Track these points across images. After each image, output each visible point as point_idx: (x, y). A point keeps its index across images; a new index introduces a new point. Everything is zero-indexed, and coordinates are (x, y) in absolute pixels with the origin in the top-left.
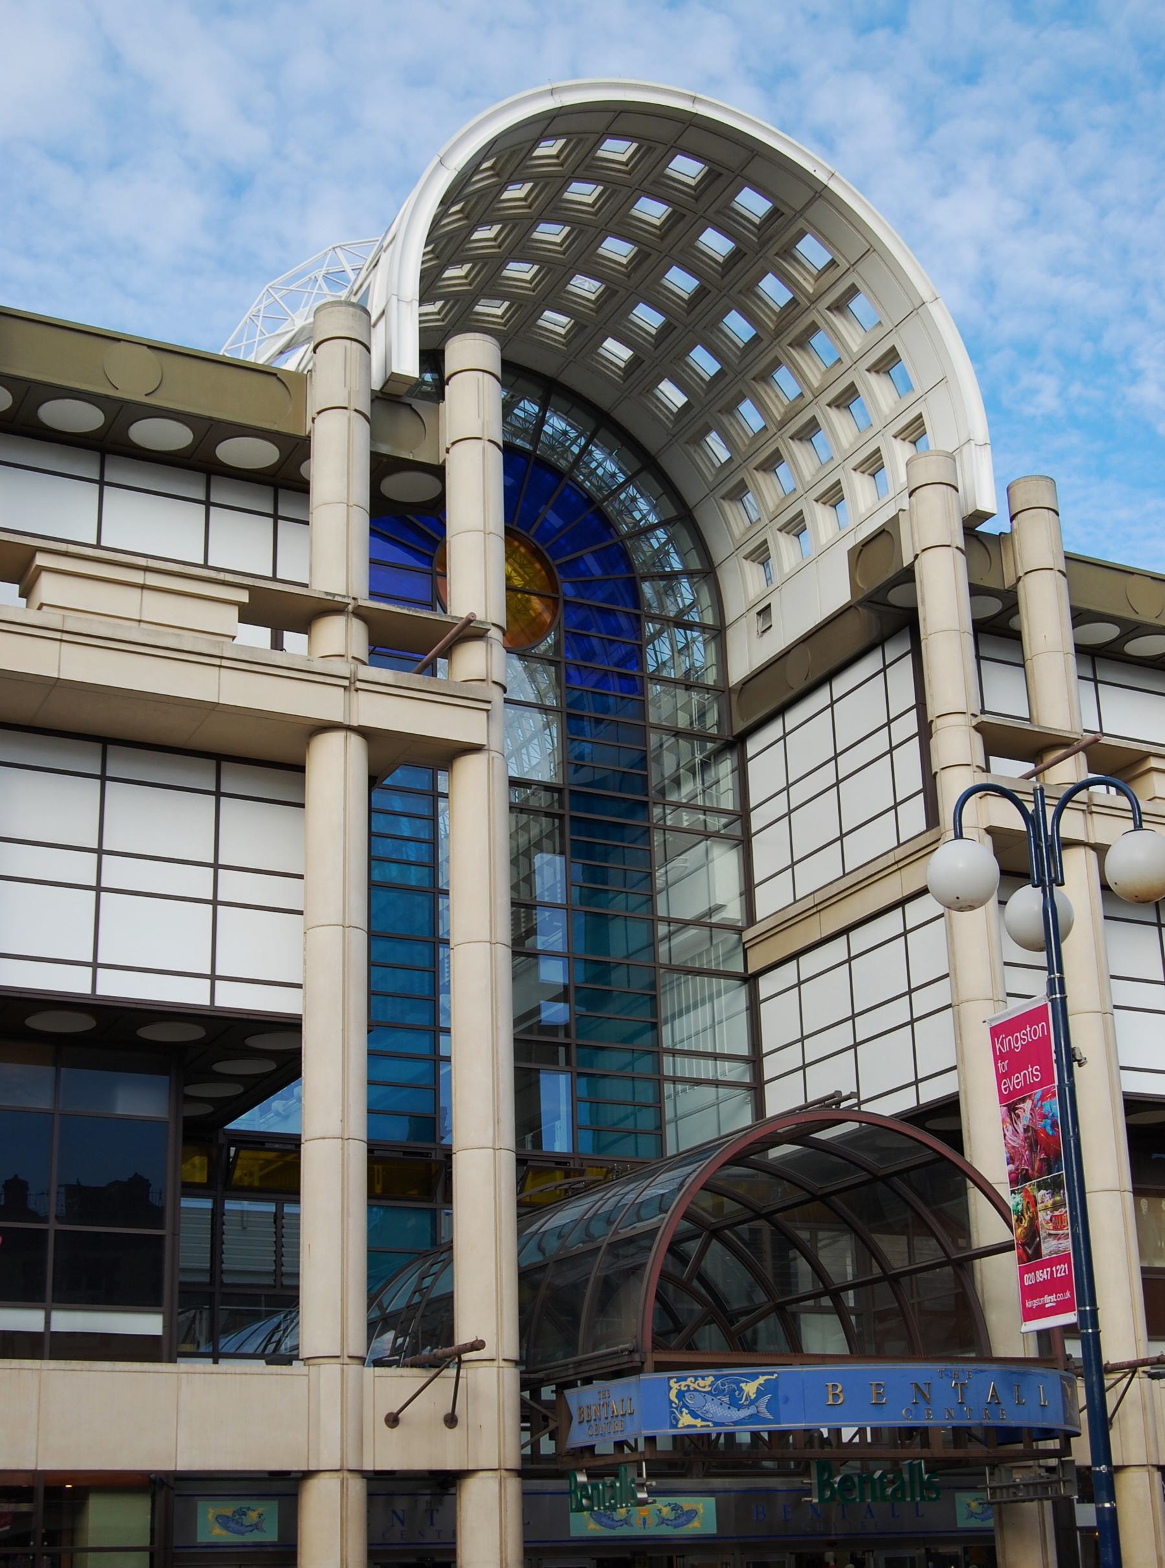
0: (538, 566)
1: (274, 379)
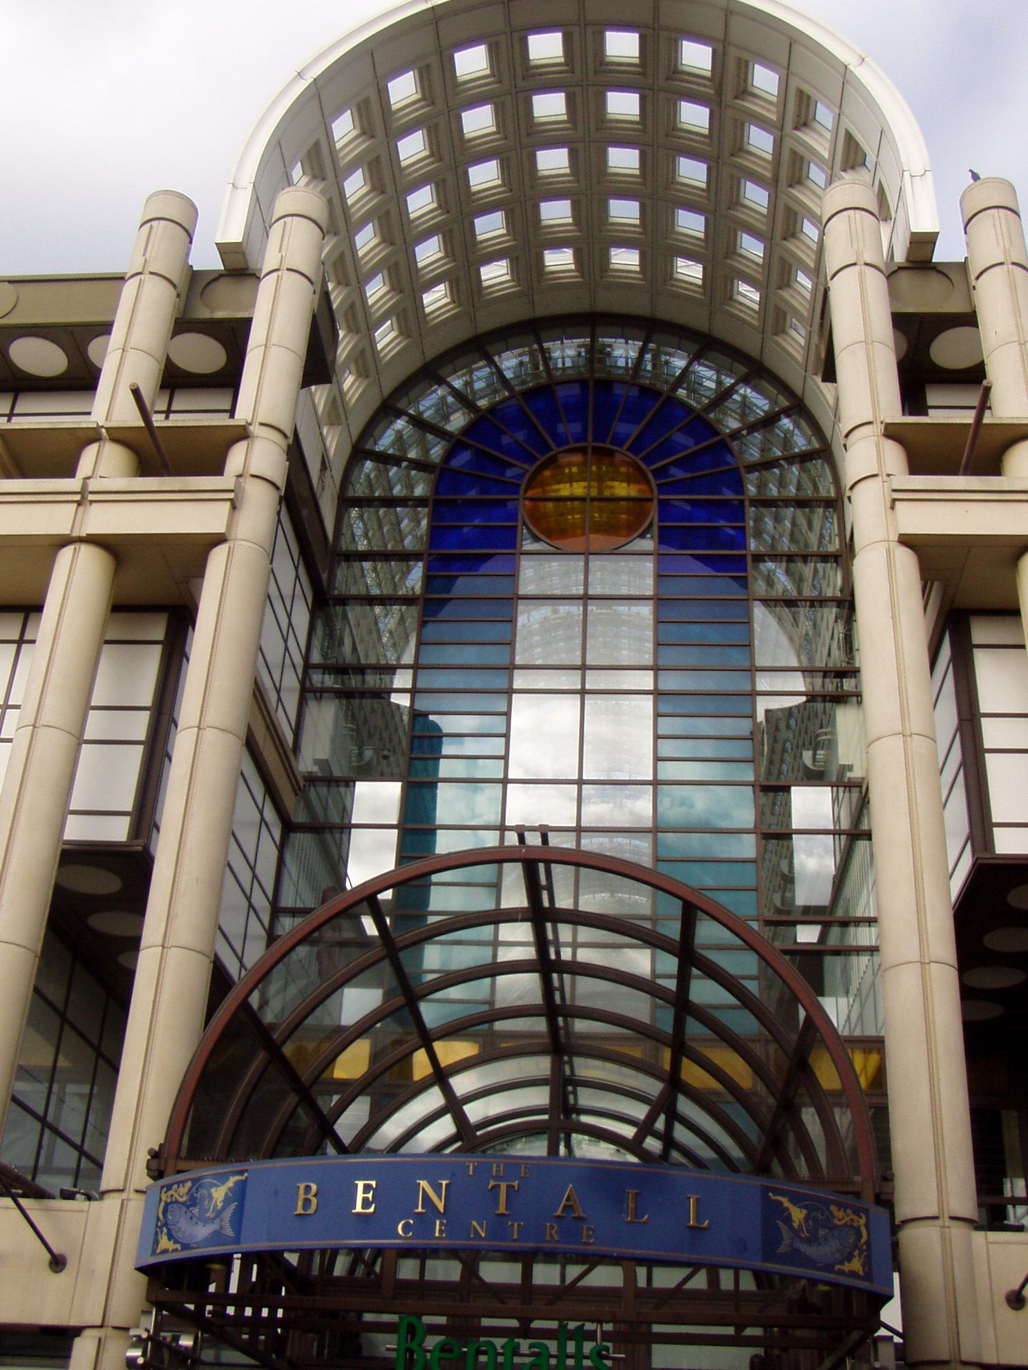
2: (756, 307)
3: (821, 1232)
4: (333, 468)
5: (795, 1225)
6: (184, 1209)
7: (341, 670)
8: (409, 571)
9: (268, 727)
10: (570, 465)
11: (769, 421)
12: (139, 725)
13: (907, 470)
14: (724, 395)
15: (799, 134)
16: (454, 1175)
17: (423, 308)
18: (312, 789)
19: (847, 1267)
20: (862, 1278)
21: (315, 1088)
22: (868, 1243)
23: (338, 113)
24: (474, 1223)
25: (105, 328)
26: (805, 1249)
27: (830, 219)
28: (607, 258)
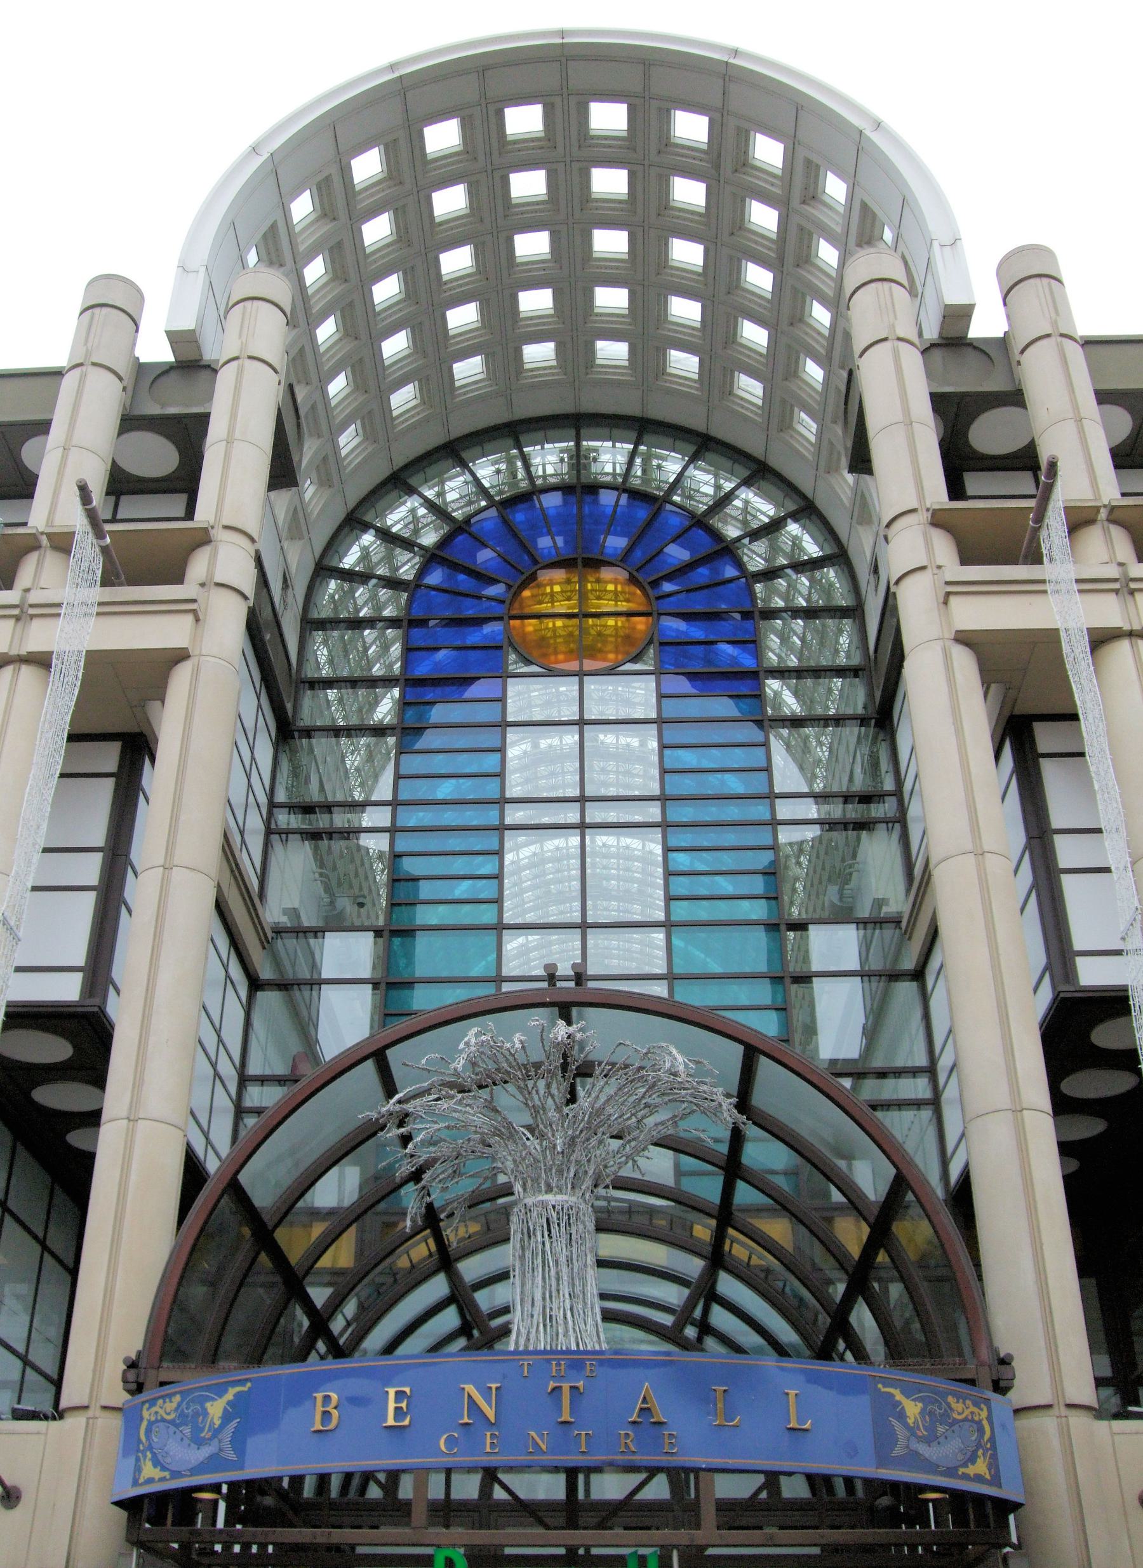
2: (760, 403)
3: (941, 1429)
4: (296, 588)
5: (911, 1421)
6: (172, 1429)
7: (308, 809)
8: (377, 702)
9: (232, 871)
10: (551, 583)
11: (774, 526)
12: (90, 869)
13: (957, 560)
14: (723, 501)
15: (806, 207)
16: (505, 1376)
17: (391, 411)
18: (279, 940)
19: (971, 1470)
20: (989, 1483)
21: (309, 1279)
22: (992, 1439)
23: (296, 193)
24: (533, 1433)
25: (43, 427)
26: (923, 1449)
27: (854, 292)
28: (591, 351)
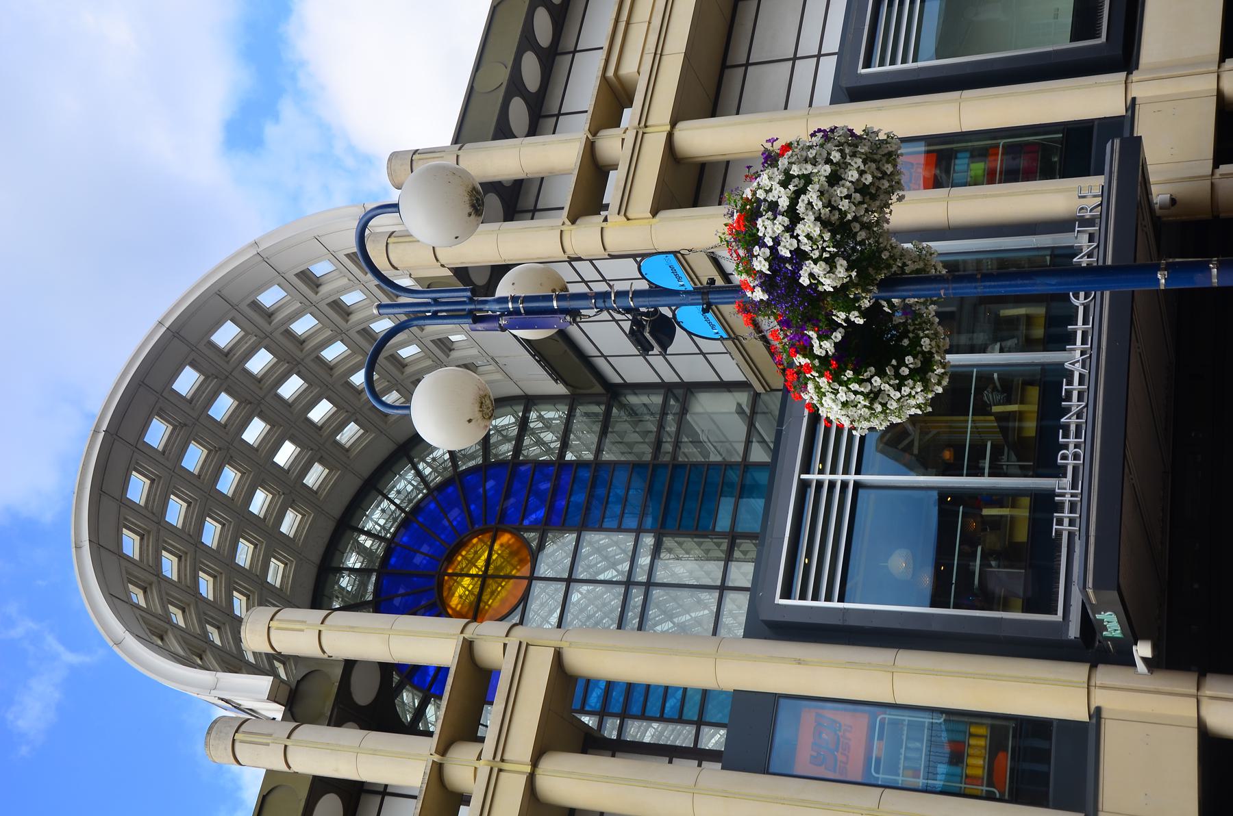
0: (475, 541)
1: (270, 799)
11: (523, 424)
